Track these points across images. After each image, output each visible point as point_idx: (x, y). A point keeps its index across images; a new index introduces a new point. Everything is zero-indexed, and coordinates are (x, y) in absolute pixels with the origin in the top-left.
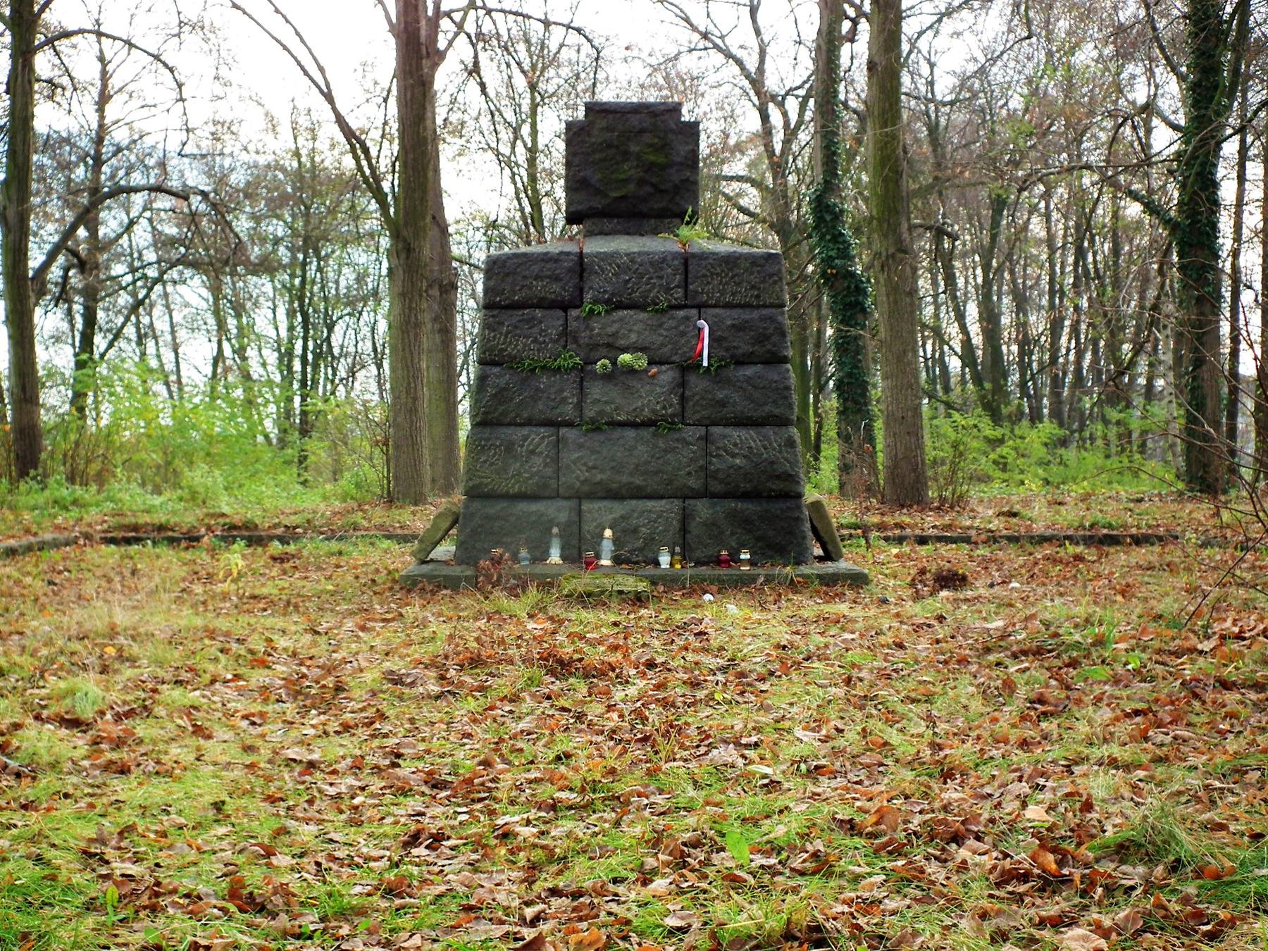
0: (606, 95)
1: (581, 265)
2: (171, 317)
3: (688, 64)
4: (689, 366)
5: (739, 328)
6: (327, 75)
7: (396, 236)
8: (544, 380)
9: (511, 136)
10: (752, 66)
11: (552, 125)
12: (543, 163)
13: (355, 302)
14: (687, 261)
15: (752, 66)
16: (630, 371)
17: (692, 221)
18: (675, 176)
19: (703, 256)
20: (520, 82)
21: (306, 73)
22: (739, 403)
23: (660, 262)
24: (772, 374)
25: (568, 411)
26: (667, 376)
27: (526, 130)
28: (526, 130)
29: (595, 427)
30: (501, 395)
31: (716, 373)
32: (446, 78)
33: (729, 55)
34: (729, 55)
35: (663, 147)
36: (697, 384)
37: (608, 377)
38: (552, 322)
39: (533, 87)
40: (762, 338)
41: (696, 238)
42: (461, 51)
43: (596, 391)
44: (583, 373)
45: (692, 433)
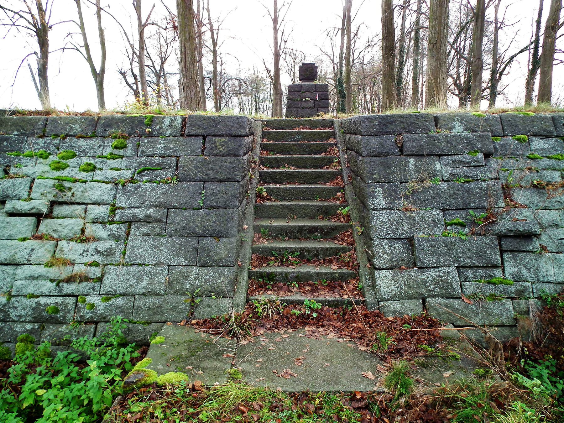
0: (306, 62)
1: (301, 86)
2: (90, 204)
3: (320, 58)
4: (315, 100)
5: (322, 95)
6: (34, 85)
7: (274, 85)
8: (296, 102)
9: (141, 292)
10: (332, 58)
11: (297, 69)
12: (296, 76)
13: (264, 100)
14: (315, 85)
15: (332, 58)
16: (308, 100)
17: (317, 80)
18: (314, 74)
19: (318, 85)
20: (292, 61)
21: (34, 79)
22: (322, 105)
23: (312, 85)
24: (326, 101)
25: (299, 106)
26: (312, 101)
27: (293, 70)
28: (293, 70)
29: (303, 108)
30: (291, 104)
31: (319, 101)
32: (281, 62)
33: (328, 56)
34: (328, 56)
35: (313, 70)
36: (316, 102)
37: (304, 101)
38: (297, 94)
39: (294, 62)
40: (325, 96)
41: (317, 82)
42: (283, 56)
43: (303, 103)
44: (301, 101)
45: (316, 109)
